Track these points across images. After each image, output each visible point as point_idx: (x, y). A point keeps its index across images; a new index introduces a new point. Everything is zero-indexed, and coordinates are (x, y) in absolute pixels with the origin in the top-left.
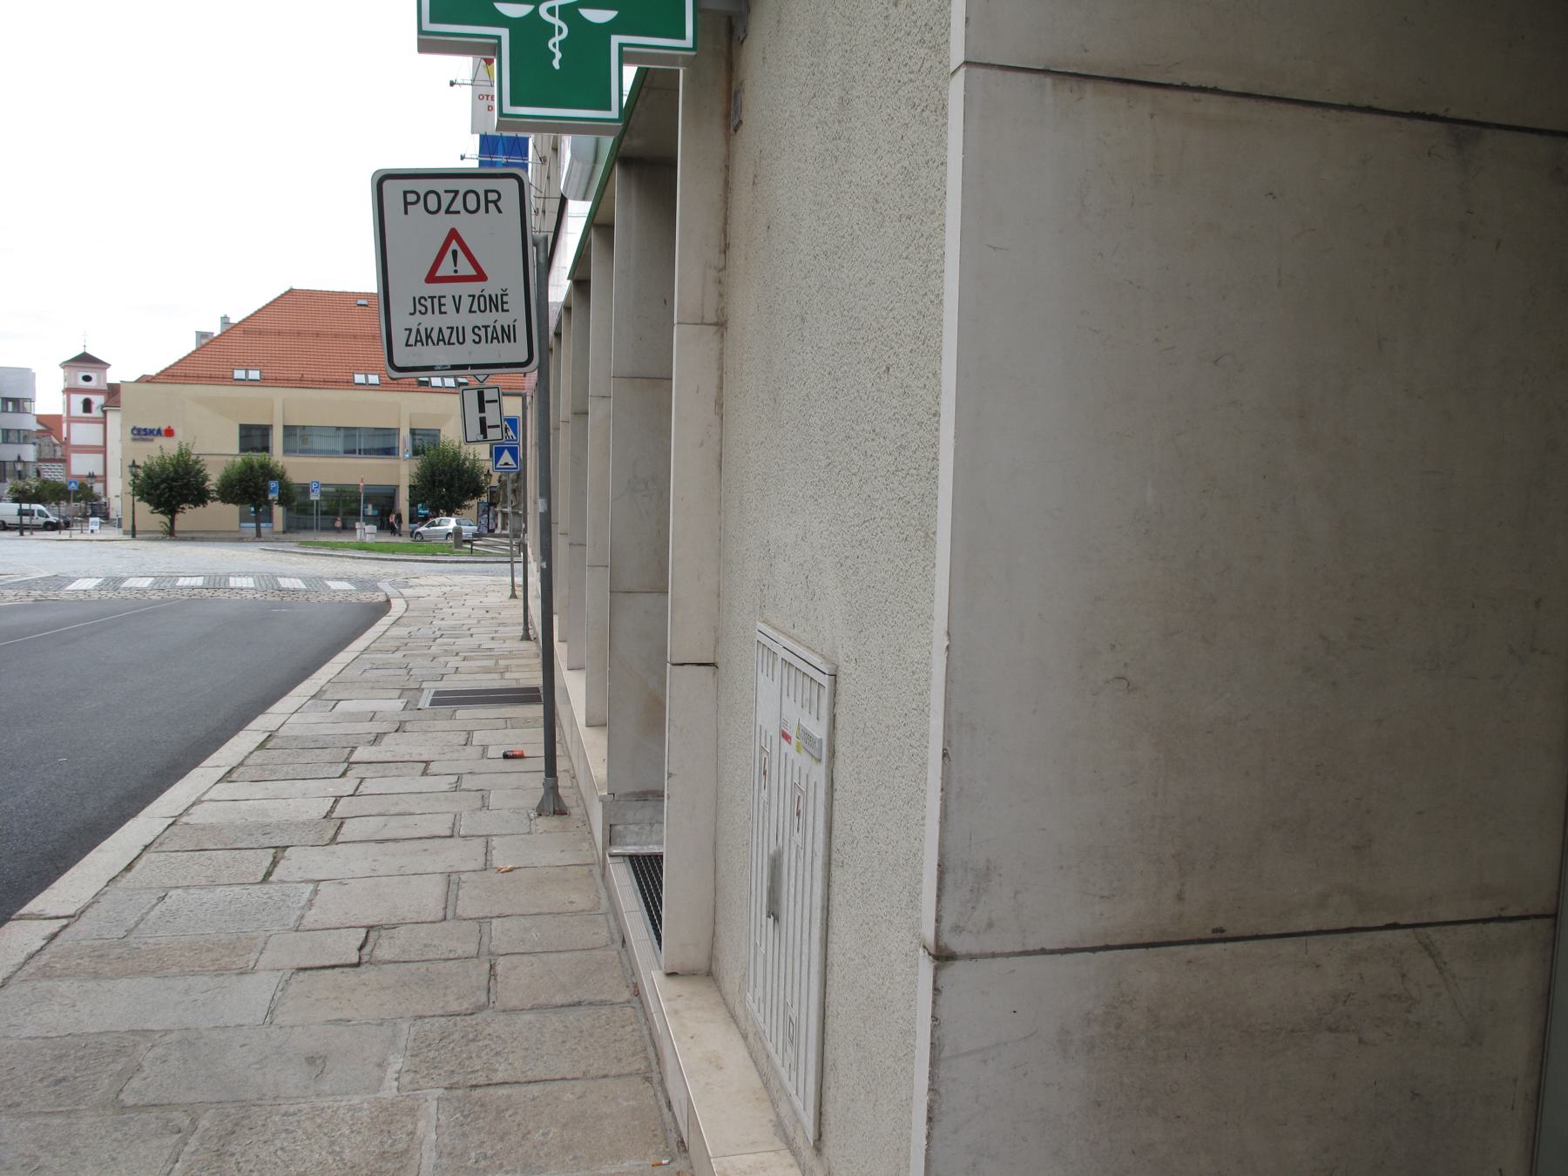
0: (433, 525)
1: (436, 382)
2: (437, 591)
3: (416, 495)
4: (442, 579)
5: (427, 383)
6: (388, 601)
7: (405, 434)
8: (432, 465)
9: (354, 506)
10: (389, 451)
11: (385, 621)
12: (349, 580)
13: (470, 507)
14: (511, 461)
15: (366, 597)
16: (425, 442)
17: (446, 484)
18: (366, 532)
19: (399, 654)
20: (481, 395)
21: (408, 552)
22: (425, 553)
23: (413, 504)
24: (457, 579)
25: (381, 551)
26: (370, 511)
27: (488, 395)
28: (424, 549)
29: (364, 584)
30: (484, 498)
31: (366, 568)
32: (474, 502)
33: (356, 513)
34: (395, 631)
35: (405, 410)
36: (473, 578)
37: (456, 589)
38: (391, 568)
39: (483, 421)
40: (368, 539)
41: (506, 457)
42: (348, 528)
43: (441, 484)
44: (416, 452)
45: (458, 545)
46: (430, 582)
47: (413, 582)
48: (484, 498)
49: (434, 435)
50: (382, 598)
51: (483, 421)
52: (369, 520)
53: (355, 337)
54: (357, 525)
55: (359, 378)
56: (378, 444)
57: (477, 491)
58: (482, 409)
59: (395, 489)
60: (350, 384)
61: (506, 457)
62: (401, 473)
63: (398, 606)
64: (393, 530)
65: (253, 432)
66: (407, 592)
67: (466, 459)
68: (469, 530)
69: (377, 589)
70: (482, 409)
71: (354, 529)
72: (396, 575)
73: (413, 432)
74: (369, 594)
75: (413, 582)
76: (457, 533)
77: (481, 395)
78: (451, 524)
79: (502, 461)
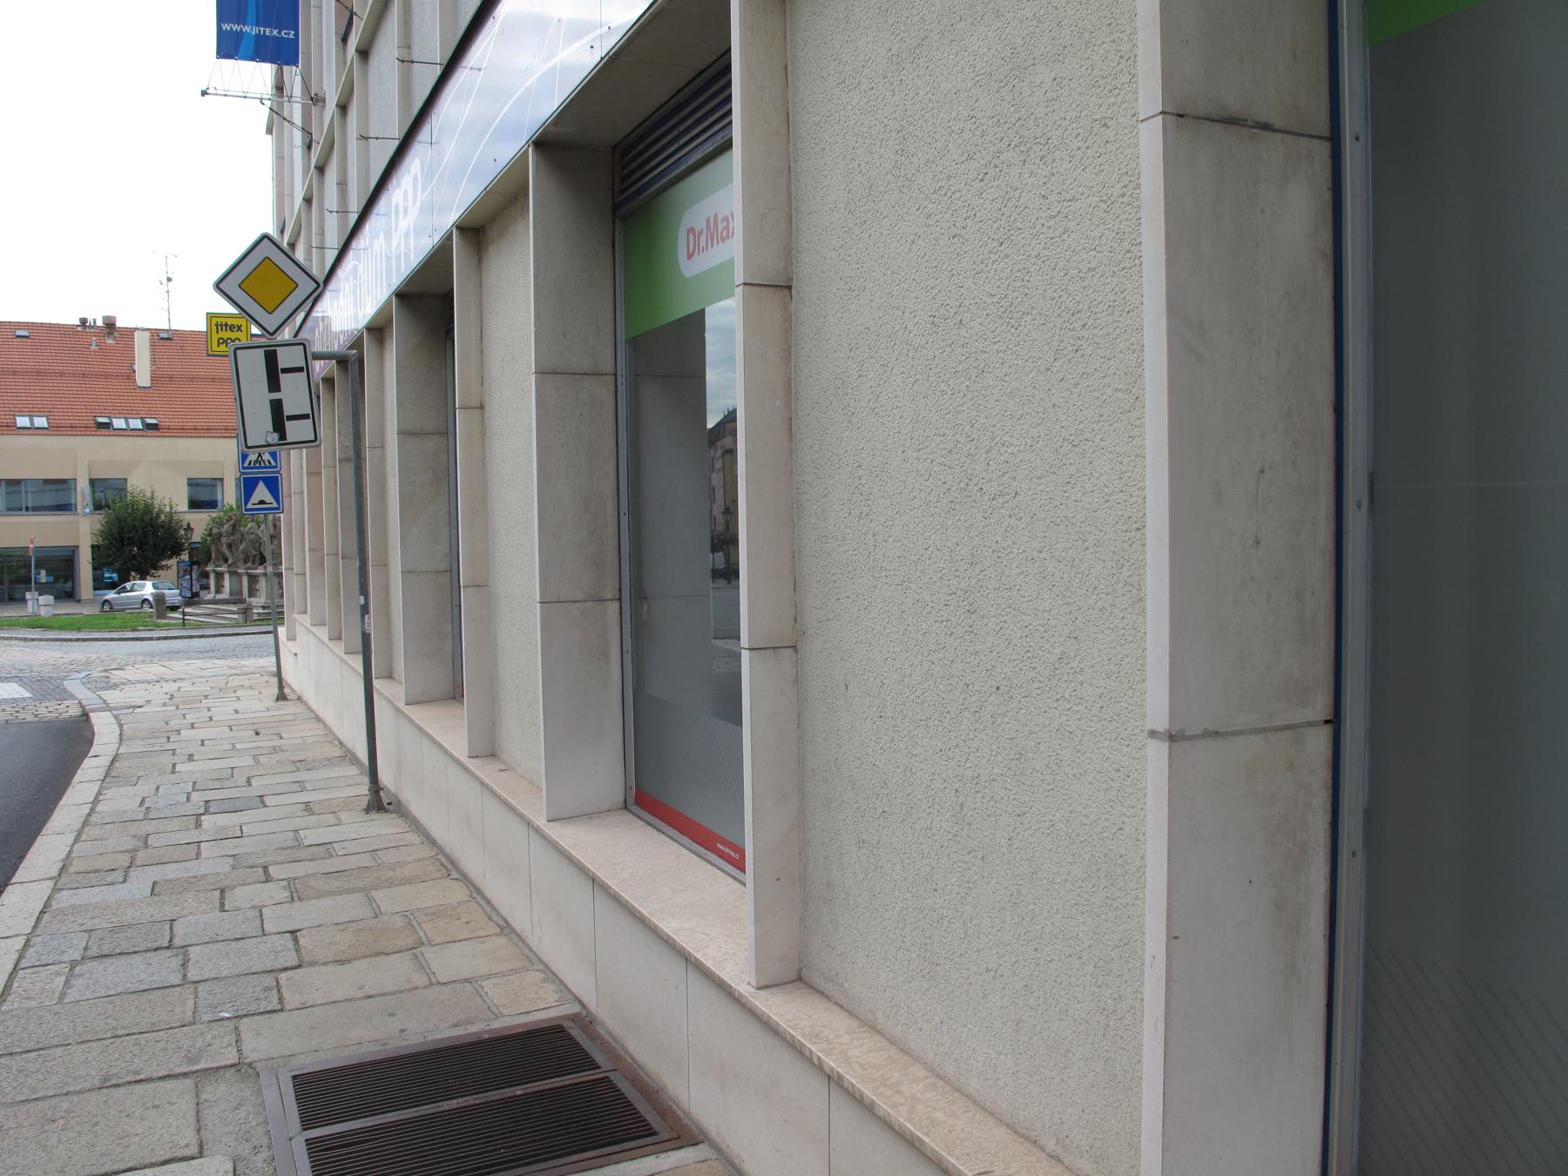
0: (125, 590)
1: (119, 423)
2: (158, 693)
3: (101, 558)
4: (155, 670)
5: (107, 426)
6: (85, 716)
7: (83, 485)
8: (119, 520)
9: (22, 572)
10: (64, 507)
11: (90, 769)
12: (19, 679)
13: (168, 568)
14: (269, 498)
15: (50, 710)
16: (107, 493)
17: (137, 540)
18: (40, 604)
19: (140, 883)
20: (271, 358)
21: (100, 630)
22: (123, 628)
23: (97, 567)
24: (179, 667)
25: (62, 628)
26: (43, 577)
27: (286, 358)
28: (117, 622)
29: (46, 686)
30: (185, 557)
31: (43, 655)
32: (173, 562)
33: (26, 581)
34: (122, 800)
35: (81, 458)
36: (200, 663)
37: (186, 686)
38: (78, 653)
39: (277, 407)
40: (43, 612)
41: (262, 492)
42: (15, 599)
43: (131, 542)
44: (98, 507)
45: (161, 615)
46: (140, 675)
47: (116, 676)
48: (185, 557)
49: (120, 486)
50: (75, 711)
51: (277, 407)
52: (42, 589)
53: (15, 373)
54: (28, 595)
55: (22, 421)
56: (49, 500)
57: (176, 550)
58: (274, 385)
59: (74, 550)
60: (10, 428)
61: (262, 492)
62: (81, 531)
63: (102, 723)
64: (70, 595)
65: (69, 584)
66: (113, 697)
67: (160, 512)
68: (173, 595)
69: (65, 695)
70: (274, 385)
71: (24, 600)
72: (88, 663)
73: (93, 482)
74: (53, 705)
75: (116, 676)
76: (160, 599)
77: (271, 358)
78: (147, 589)
79: (255, 498)
